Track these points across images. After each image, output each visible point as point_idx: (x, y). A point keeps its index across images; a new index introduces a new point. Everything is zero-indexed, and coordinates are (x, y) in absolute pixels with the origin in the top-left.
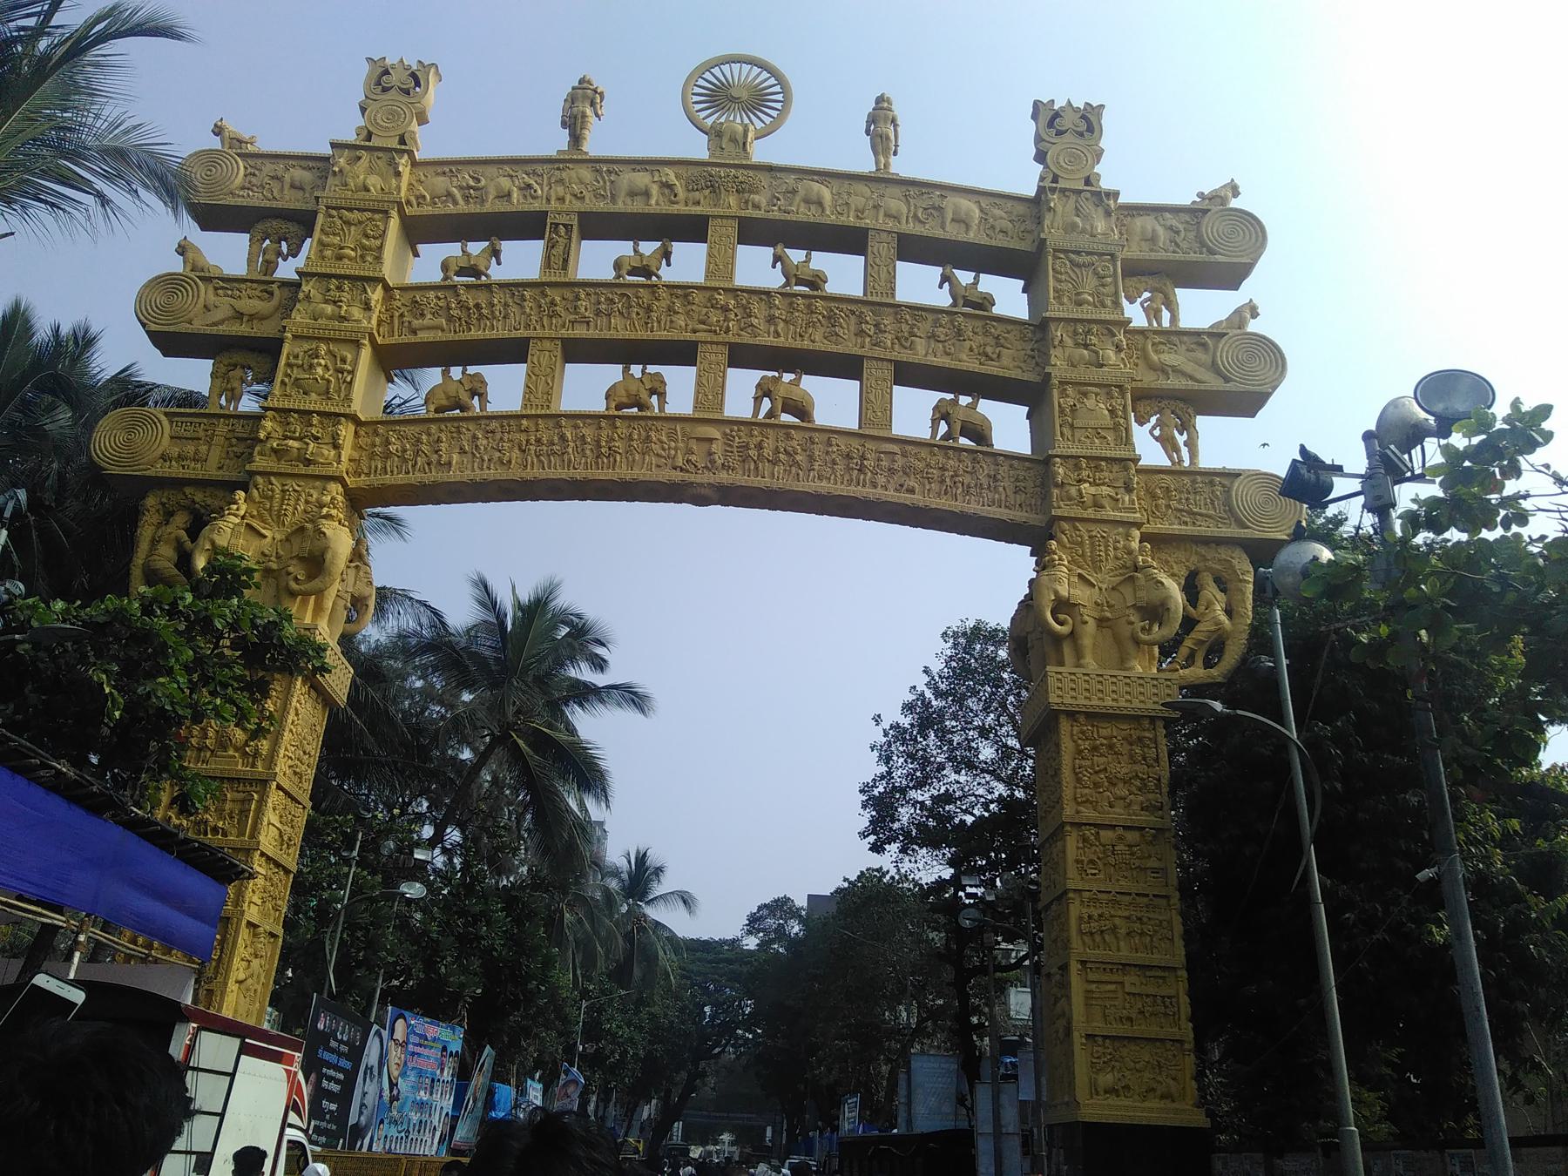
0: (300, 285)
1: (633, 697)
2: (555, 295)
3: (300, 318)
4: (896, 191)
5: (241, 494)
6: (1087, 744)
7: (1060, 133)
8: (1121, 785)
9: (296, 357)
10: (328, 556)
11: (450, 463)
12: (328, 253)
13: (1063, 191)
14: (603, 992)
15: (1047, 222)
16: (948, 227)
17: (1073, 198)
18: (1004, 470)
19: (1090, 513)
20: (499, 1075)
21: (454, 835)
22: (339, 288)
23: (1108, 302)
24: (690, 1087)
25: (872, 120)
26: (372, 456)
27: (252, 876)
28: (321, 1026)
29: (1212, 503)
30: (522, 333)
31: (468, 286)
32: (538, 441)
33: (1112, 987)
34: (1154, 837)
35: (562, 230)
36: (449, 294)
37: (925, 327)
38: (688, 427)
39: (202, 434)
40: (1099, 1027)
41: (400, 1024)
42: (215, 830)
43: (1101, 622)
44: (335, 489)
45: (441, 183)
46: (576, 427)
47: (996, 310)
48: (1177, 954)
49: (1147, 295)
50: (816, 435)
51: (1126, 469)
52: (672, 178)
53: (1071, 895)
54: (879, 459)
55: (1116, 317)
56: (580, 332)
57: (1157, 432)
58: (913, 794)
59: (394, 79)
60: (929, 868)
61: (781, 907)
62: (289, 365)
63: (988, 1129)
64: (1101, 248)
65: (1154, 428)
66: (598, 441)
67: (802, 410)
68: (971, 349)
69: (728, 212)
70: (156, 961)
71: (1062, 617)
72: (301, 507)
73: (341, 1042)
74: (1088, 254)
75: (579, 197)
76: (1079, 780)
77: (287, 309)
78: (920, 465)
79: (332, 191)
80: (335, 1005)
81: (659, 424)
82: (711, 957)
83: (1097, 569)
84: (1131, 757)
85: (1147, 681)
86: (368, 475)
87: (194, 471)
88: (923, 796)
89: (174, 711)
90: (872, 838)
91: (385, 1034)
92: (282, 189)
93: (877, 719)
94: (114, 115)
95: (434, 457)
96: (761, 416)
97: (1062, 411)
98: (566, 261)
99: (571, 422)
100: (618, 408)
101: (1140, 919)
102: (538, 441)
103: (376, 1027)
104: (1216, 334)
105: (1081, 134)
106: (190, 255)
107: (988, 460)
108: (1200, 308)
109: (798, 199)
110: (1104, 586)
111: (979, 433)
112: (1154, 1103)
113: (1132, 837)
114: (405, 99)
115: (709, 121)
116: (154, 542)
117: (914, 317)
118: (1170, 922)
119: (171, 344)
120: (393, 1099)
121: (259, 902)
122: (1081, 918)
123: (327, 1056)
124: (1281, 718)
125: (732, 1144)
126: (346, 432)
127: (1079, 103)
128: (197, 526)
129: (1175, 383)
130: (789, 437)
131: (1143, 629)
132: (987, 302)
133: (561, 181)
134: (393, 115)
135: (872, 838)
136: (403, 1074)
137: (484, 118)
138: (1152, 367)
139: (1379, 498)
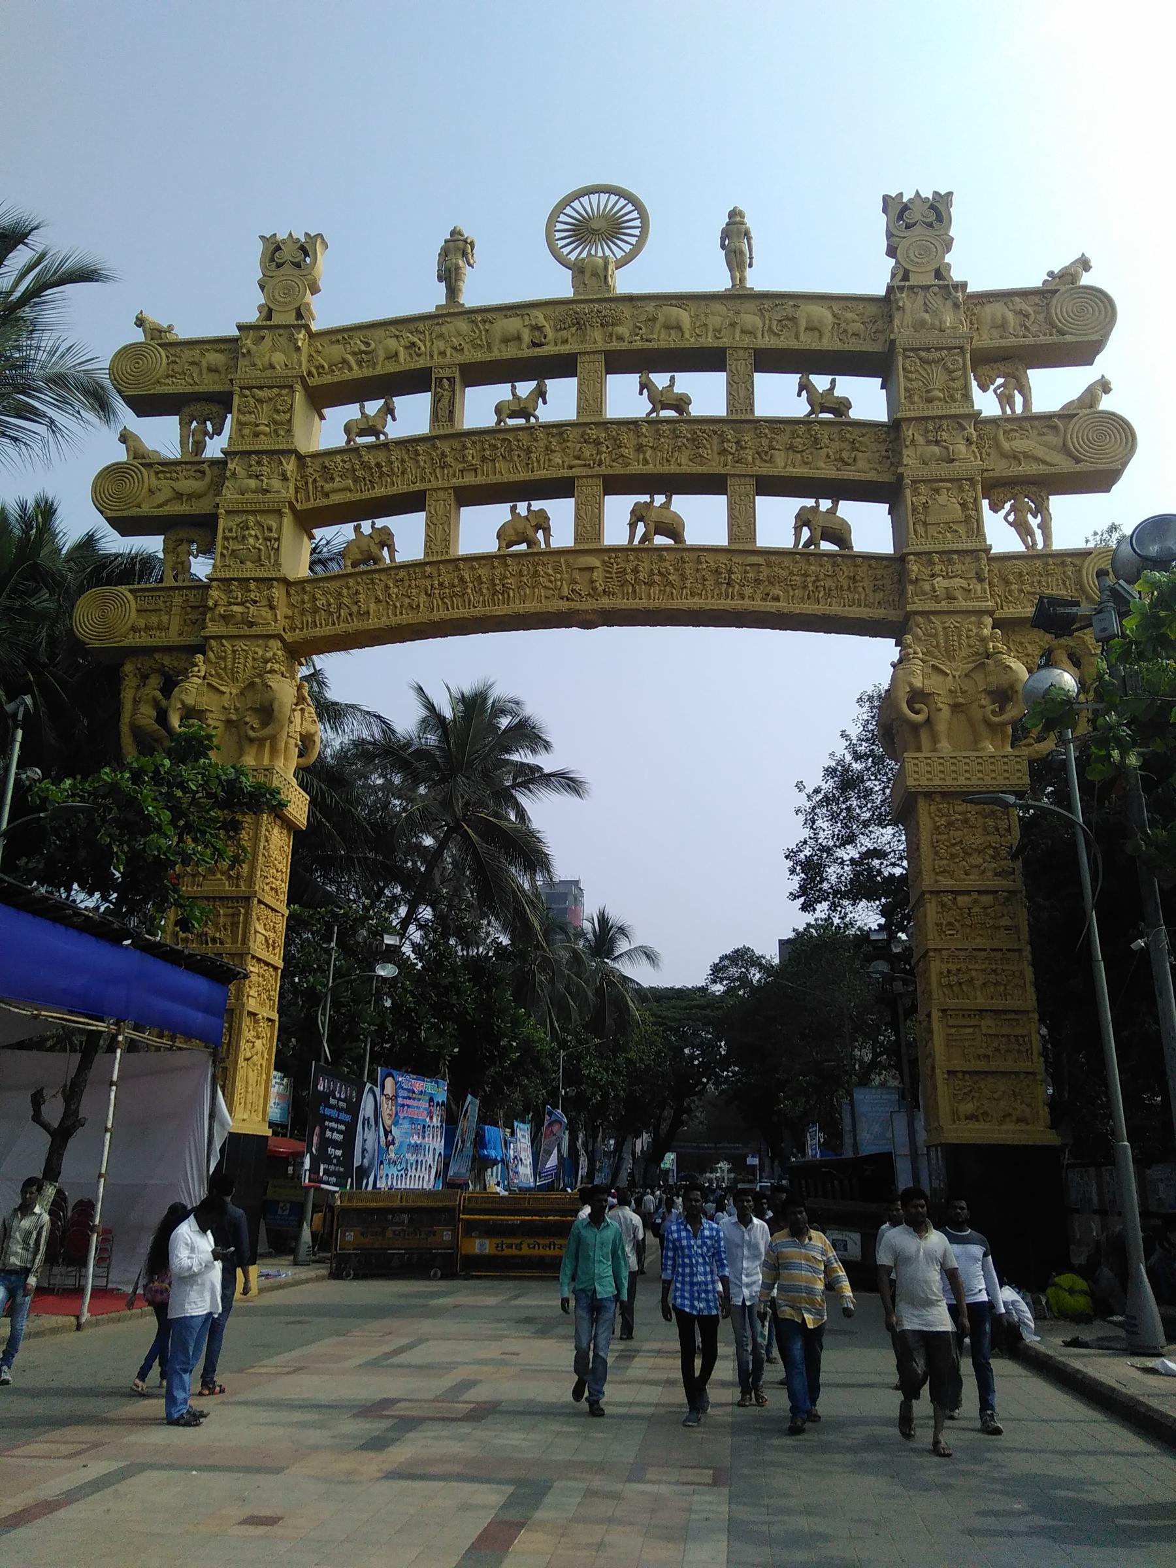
0: (226, 464)
1: (569, 783)
2: (445, 446)
3: (229, 493)
4: (751, 306)
5: (200, 657)
6: (943, 821)
7: (908, 226)
8: (975, 855)
9: (231, 530)
10: (276, 706)
11: (368, 613)
12: (246, 431)
13: (911, 288)
14: (580, 1042)
15: (896, 322)
16: (802, 338)
17: (921, 293)
18: (862, 571)
19: (944, 605)
20: (487, 1118)
21: (426, 913)
22: (259, 463)
23: (958, 396)
24: (677, 1123)
25: (726, 234)
26: (303, 612)
27: (246, 976)
28: (320, 1088)
29: (1064, 583)
30: (419, 486)
31: (369, 447)
32: (441, 585)
33: (971, 1030)
34: (1007, 899)
35: (446, 383)
36: (353, 456)
37: (784, 438)
38: (571, 559)
39: (162, 605)
40: (959, 1064)
41: (389, 1082)
42: (214, 940)
43: (955, 708)
44: (275, 644)
45: (336, 351)
46: (473, 568)
47: (854, 414)
48: (1030, 999)
49: (1000, 381)
50: (686, 555)
51: (978, 560)
52: (542, 321)
53: (931, 954)
54: (746, 572)
55: (966, 411)
56: (469, 479)
57: (1011, 518)
58: (840, 853)
59: (286, 254)
60: (867, 916)
61: (742, 957)
62: (226, 538)
63: (906, 1151)
64: (951, 342)
65: (1008, 514)
66: (493, 580)
67: (674, 530)
68: (828, 456)
69: (594, 347)
70: (180, 1049)
71: (917, 706)
72: (250, 663)
73: (339, 1099)
74: (937, 349)
75: (458, 349)
76: (937, 853)
77: (217, 486)
78: (784, 573)
79: (244, 372)
80: (332, 1070)
81: (545, 559)
82: (684, 1004)
83: (952, 658)
84: (985, 829)
85: (999, 763)
86: (301, 629)
87: (160, 639)
88: (850, 852)
89: (168, 858)
90: (802, 900)
91: (377, 1090)
92: (201, 373)
93: (800, 786)
94: (50, 344)
95: (355, 608)
96: (636, 542)
97: (914, 510)
98: (451, 412)
99: (468, 565)
100: (509, 546)
101: (994, 971)
102: (441, 585)
103: (368, 1086)
104: (1067, 415)
105: (930, 225)
106: (131, 443)
107: (849, 561)
108: (1052, 389)
109: (658, 325)
110: (957, 674)
111: (839, 534)
112: (1009, 1126)
113: (986, 900)
114: (296, 271)
115: (573, 257)
116: (136, 702)
117: (773, 431)
118: (1022, 973)
119: (126, 526)
120: (388, 1144)
121: (256, 995)
122: (942, 973)
123: (328, 1112)
124: (1070, 807)
125: (730, 1171)
126: (278, 593)
127: (927, 194)
128: (169, 685)
129: (1027, 469)
130: (662, 559)
131: (993, 712)
132: (842, 406)
133: (441, 336)
134: (288, 291)
135: (802, 900)
136: (396, 1123)
137: (369, 285)
138: (1004, 455)
139: (1104, 630)
